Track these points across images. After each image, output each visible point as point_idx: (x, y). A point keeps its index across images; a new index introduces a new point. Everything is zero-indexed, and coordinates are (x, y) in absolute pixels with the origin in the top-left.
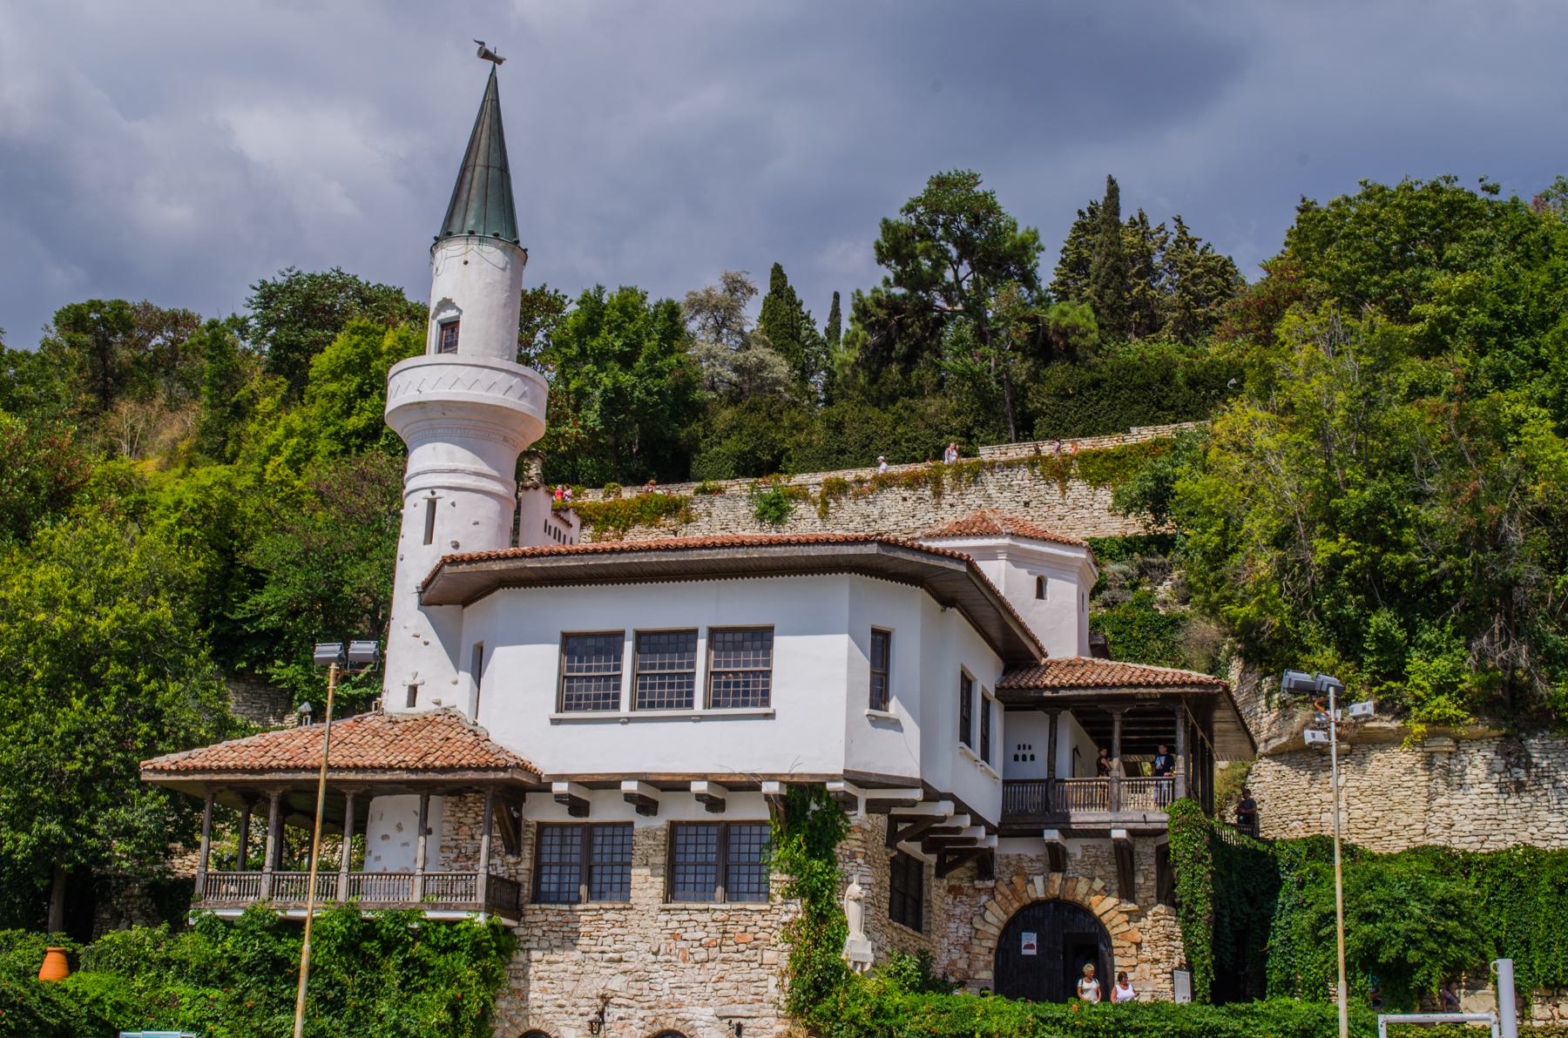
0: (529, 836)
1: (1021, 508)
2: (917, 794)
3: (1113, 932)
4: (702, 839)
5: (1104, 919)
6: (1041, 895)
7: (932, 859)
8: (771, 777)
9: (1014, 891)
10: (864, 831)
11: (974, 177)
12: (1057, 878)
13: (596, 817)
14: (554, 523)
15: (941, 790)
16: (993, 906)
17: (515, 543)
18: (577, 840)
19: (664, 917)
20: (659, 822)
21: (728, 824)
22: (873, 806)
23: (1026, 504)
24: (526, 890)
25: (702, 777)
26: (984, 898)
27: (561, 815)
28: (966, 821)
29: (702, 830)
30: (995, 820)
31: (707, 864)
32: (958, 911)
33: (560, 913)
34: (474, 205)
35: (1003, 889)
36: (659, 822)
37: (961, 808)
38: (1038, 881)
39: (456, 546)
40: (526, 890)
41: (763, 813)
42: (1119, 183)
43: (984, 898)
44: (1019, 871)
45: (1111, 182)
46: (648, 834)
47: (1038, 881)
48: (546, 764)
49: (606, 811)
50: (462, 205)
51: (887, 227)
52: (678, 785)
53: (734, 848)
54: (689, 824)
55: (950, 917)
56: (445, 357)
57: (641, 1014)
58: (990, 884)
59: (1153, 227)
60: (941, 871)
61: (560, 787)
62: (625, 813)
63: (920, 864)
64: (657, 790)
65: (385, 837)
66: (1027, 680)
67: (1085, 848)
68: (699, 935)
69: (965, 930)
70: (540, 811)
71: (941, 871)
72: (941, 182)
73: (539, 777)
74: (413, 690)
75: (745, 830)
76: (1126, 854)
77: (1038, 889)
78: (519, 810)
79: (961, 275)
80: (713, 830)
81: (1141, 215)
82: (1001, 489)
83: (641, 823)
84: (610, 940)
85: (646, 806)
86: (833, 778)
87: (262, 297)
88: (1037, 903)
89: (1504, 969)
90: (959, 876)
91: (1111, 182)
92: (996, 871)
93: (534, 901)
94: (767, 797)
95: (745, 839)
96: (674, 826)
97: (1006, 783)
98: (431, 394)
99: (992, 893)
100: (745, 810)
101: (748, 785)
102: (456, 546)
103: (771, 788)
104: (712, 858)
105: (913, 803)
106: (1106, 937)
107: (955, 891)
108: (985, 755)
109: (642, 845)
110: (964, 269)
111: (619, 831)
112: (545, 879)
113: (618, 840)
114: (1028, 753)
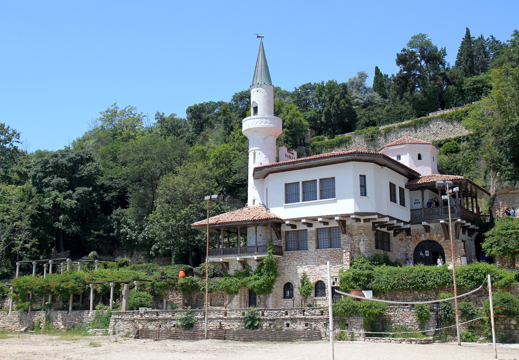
0: (283, 235)
1: (439, 130)
2: (376, 216)
3: (444, 248)
4: (324, 232)
5: (442, 244)
6: (424, 239)
7: (392, 232)
8: (337, 216)
9: (416, 239)
10: (363, 227)
11: (425, 35)
12: (428, 234)
13: (298, 228)
14: (288, 154)
15: (385, 215)
16: (411, 243)
17: (278, 161)
18: (327, 232)
19: (316, 253)
20: (313, 229)
21: (330, 228)
22: (365, 220)
23: (441, 128)
24: (284, 248)
25: (321, 217)
26: (409, 241)
27: (289, 229)
28: (395, 221)
29: (324, 230)
30: (408, 220)
31: (326, 238)
32: (402, 245)
33: (292, 253)
34: (259, 76)
35: (414, 238)
36: (313, 229)
37: (391, 218)
38: (423, 235)
39: (261, 163)
40: (284, 248)
41: (336, 225)
42: (470, 29)
43: (409, 241)
44: (418, 233)
45: (467, 29)
46: (311, 232)
47: (423, 235)
48: (283, 217)
49: (300, 227)
50: (256, 77)
51: (398, 55)
52: (315, 219)
53: (300, 237)
54: (321, 228)
55: (400, 246)
56: (255, 117)
57: (313, 277)
58: (410, 237)
59: (485, 39)
60: (395, 234)
61: (287, 222)
62: (305, 227)
63: (389, 234)
64: (310, 222)
65: (250, 237)
66: (413, 183)
67: (435, 226)
68: (325, 256)
69: (404, 250)
70: (284, 229)
71: (395, 234)
72: (415, 37)
73: (282, 220)
74: (254, 200)
75: (302, 232)
76: (445, 227)
77: (423, 238)
78: (280, 228)
79: (422, 64)
80: (327, 230)
81: (482, 36)
82: (434, 125)
83: (309, 229)
84: (304, 259)
85: (310, 225)
86: (352, 214)
87: (159, 122)
88: (423, 241)
89: (328, 262)
90: (402, 235)
91: (467, 29)
92: (412, 233)
93: (286, 250)
94: (336, 220)
95: (335, 231)
96: (317, 229)
97: (411, 210)
98: (254, 126)
99: (411, 239)
100: (333, 224)
101: (332, 218)
102: (261, 163)
103: (337, 218)
104: (327, 237)
105: (375, 219)
106: (442, 249)
107: (401, 239)
108: (403, 203)
109: (310, 235)
110: (423, 63)
111: (304, 232)
112: (320, 242)
113: (304, 234)
114: (418, 202)
